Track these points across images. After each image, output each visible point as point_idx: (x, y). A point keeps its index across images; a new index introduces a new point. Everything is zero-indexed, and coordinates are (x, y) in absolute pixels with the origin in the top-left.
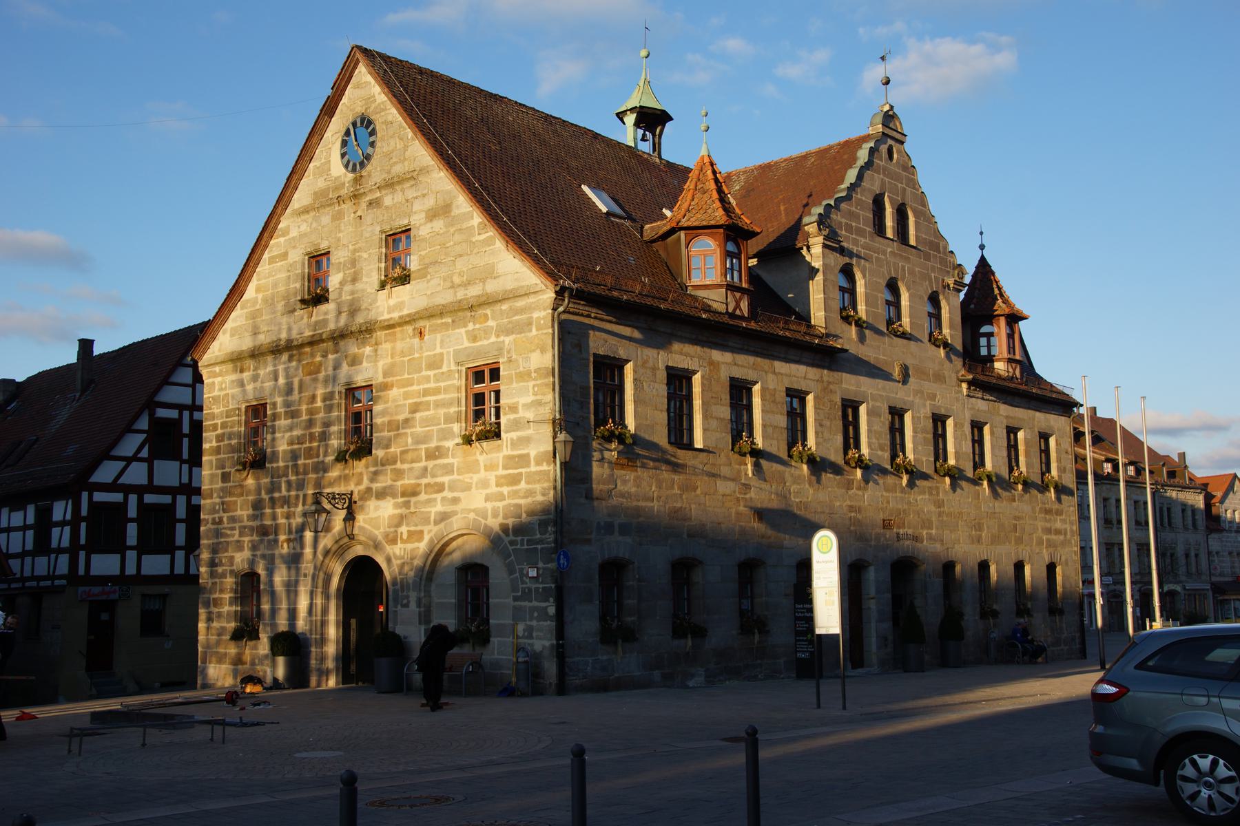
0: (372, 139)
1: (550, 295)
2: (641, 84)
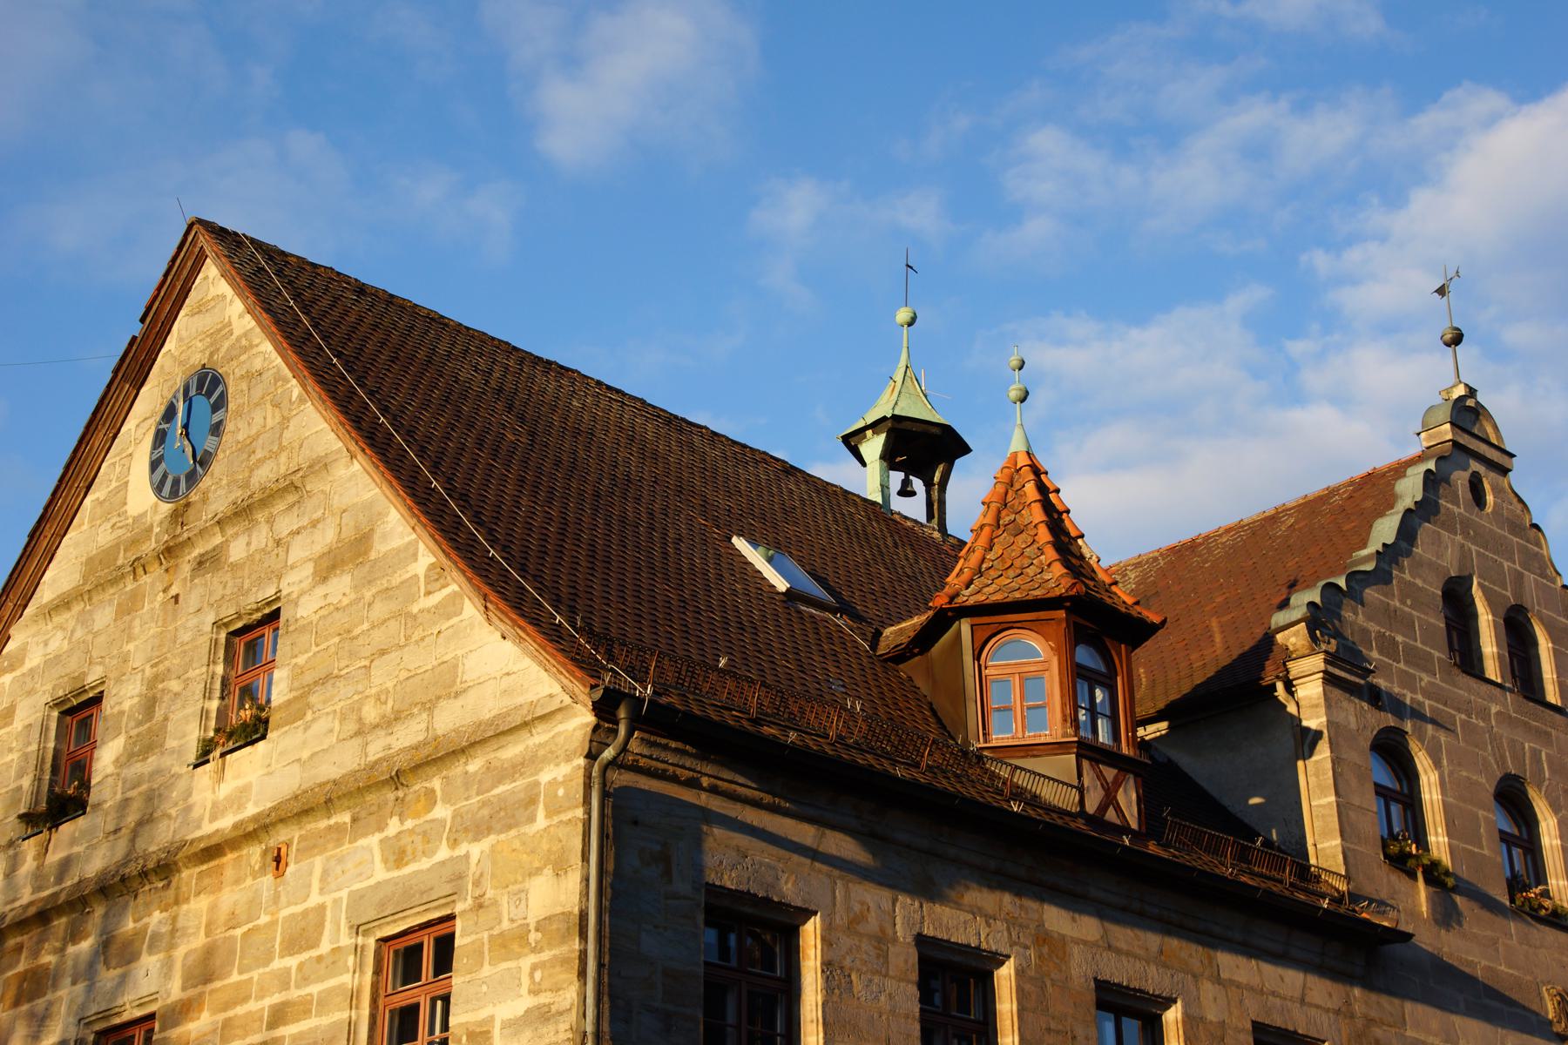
0: (216, 418)
1: (585, 718)
2: (899, 377)
